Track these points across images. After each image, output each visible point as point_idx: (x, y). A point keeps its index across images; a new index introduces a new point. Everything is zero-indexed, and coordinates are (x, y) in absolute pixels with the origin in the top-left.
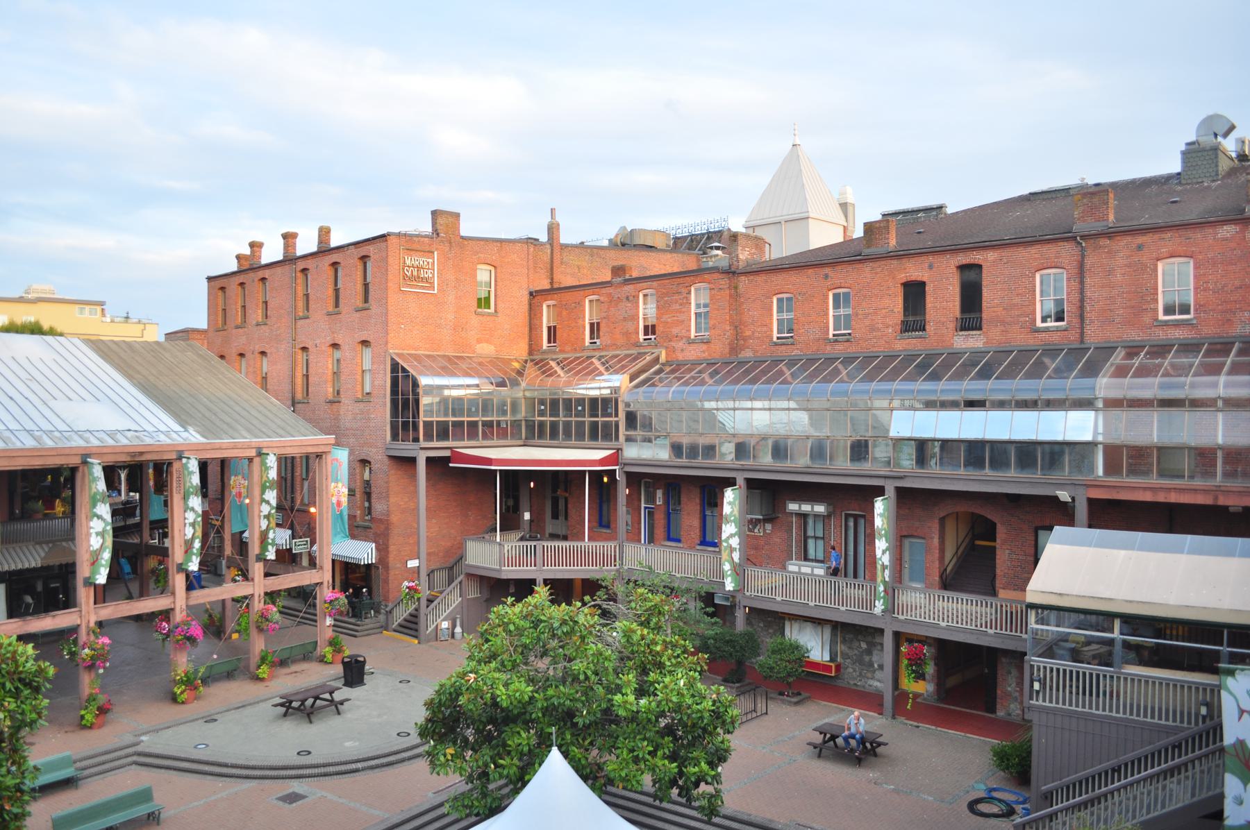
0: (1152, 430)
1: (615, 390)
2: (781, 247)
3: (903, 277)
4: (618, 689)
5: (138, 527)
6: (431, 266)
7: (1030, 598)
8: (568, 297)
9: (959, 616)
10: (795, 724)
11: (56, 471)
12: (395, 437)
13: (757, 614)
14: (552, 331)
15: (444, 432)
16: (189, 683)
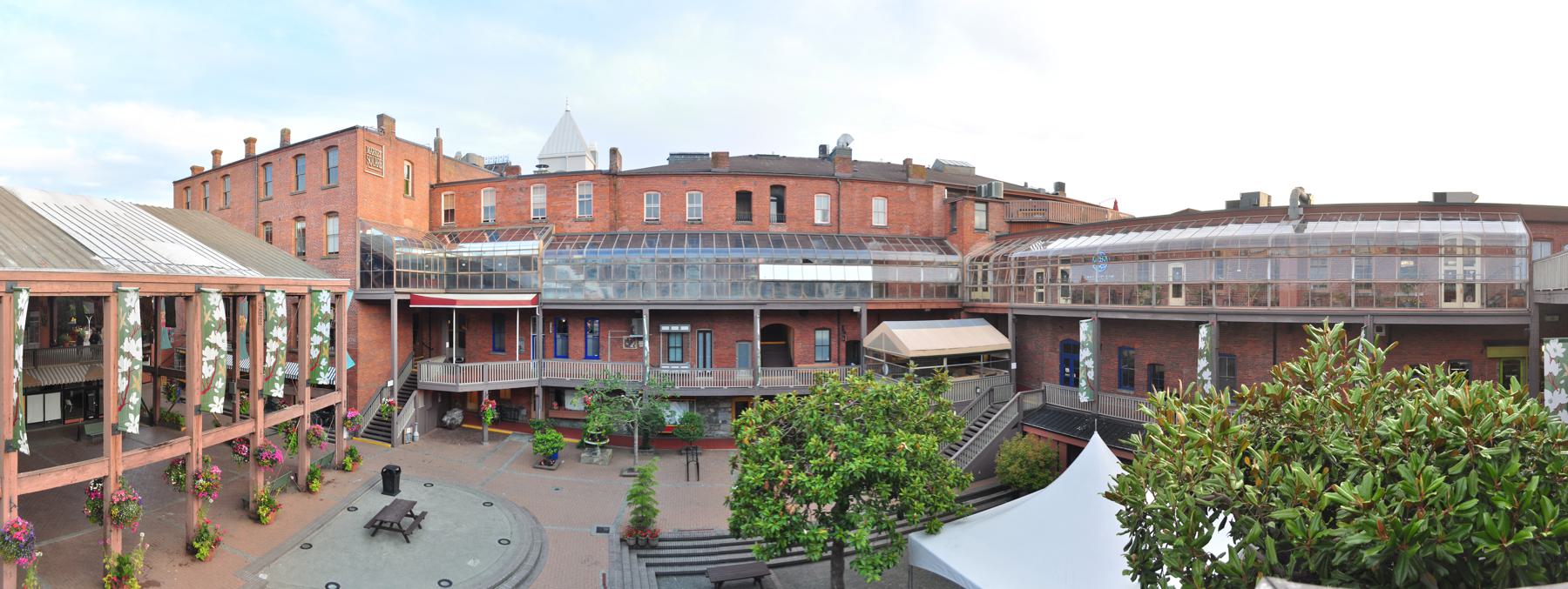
0: (895, 275)
3: (738, 188)
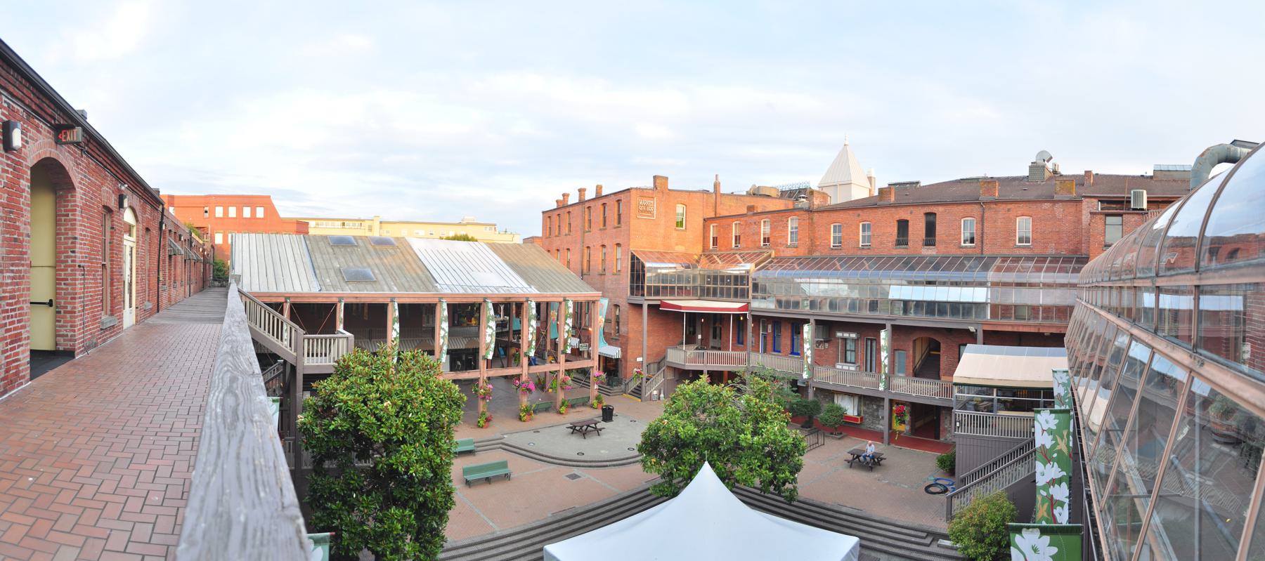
0: (1014, 297)
1: (748, 272)
2: (837, 199)
3: (898, 217)
4: (743, 431)
5: (508, 332)
6: (653, 204)
7: (955, 380)
8: (724, 222)
9: (922, 391)
10: (835, 451)
11: (473, 305)
12: (632, 293)
13: (819, 391)
14: (715, 239)
15: (657, 291)
16: (527, 411)
